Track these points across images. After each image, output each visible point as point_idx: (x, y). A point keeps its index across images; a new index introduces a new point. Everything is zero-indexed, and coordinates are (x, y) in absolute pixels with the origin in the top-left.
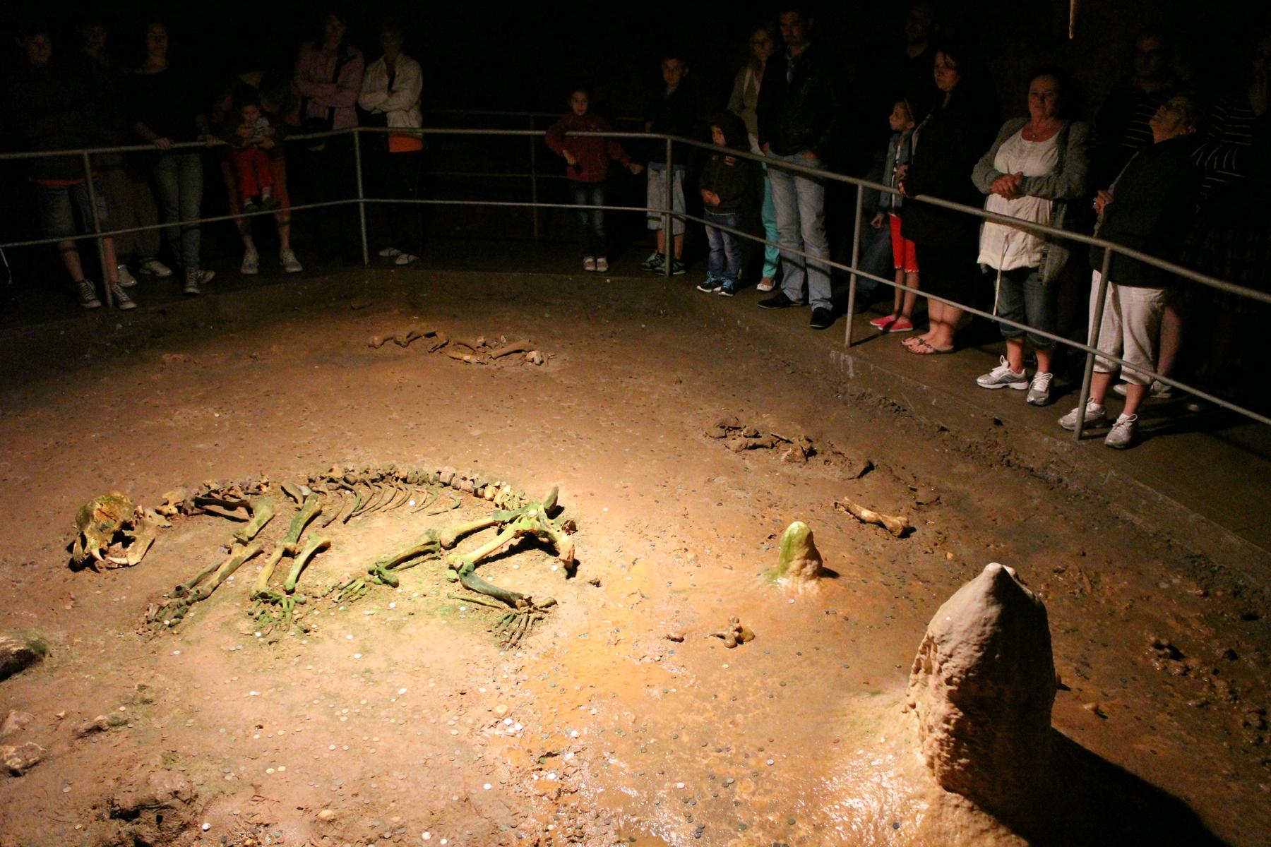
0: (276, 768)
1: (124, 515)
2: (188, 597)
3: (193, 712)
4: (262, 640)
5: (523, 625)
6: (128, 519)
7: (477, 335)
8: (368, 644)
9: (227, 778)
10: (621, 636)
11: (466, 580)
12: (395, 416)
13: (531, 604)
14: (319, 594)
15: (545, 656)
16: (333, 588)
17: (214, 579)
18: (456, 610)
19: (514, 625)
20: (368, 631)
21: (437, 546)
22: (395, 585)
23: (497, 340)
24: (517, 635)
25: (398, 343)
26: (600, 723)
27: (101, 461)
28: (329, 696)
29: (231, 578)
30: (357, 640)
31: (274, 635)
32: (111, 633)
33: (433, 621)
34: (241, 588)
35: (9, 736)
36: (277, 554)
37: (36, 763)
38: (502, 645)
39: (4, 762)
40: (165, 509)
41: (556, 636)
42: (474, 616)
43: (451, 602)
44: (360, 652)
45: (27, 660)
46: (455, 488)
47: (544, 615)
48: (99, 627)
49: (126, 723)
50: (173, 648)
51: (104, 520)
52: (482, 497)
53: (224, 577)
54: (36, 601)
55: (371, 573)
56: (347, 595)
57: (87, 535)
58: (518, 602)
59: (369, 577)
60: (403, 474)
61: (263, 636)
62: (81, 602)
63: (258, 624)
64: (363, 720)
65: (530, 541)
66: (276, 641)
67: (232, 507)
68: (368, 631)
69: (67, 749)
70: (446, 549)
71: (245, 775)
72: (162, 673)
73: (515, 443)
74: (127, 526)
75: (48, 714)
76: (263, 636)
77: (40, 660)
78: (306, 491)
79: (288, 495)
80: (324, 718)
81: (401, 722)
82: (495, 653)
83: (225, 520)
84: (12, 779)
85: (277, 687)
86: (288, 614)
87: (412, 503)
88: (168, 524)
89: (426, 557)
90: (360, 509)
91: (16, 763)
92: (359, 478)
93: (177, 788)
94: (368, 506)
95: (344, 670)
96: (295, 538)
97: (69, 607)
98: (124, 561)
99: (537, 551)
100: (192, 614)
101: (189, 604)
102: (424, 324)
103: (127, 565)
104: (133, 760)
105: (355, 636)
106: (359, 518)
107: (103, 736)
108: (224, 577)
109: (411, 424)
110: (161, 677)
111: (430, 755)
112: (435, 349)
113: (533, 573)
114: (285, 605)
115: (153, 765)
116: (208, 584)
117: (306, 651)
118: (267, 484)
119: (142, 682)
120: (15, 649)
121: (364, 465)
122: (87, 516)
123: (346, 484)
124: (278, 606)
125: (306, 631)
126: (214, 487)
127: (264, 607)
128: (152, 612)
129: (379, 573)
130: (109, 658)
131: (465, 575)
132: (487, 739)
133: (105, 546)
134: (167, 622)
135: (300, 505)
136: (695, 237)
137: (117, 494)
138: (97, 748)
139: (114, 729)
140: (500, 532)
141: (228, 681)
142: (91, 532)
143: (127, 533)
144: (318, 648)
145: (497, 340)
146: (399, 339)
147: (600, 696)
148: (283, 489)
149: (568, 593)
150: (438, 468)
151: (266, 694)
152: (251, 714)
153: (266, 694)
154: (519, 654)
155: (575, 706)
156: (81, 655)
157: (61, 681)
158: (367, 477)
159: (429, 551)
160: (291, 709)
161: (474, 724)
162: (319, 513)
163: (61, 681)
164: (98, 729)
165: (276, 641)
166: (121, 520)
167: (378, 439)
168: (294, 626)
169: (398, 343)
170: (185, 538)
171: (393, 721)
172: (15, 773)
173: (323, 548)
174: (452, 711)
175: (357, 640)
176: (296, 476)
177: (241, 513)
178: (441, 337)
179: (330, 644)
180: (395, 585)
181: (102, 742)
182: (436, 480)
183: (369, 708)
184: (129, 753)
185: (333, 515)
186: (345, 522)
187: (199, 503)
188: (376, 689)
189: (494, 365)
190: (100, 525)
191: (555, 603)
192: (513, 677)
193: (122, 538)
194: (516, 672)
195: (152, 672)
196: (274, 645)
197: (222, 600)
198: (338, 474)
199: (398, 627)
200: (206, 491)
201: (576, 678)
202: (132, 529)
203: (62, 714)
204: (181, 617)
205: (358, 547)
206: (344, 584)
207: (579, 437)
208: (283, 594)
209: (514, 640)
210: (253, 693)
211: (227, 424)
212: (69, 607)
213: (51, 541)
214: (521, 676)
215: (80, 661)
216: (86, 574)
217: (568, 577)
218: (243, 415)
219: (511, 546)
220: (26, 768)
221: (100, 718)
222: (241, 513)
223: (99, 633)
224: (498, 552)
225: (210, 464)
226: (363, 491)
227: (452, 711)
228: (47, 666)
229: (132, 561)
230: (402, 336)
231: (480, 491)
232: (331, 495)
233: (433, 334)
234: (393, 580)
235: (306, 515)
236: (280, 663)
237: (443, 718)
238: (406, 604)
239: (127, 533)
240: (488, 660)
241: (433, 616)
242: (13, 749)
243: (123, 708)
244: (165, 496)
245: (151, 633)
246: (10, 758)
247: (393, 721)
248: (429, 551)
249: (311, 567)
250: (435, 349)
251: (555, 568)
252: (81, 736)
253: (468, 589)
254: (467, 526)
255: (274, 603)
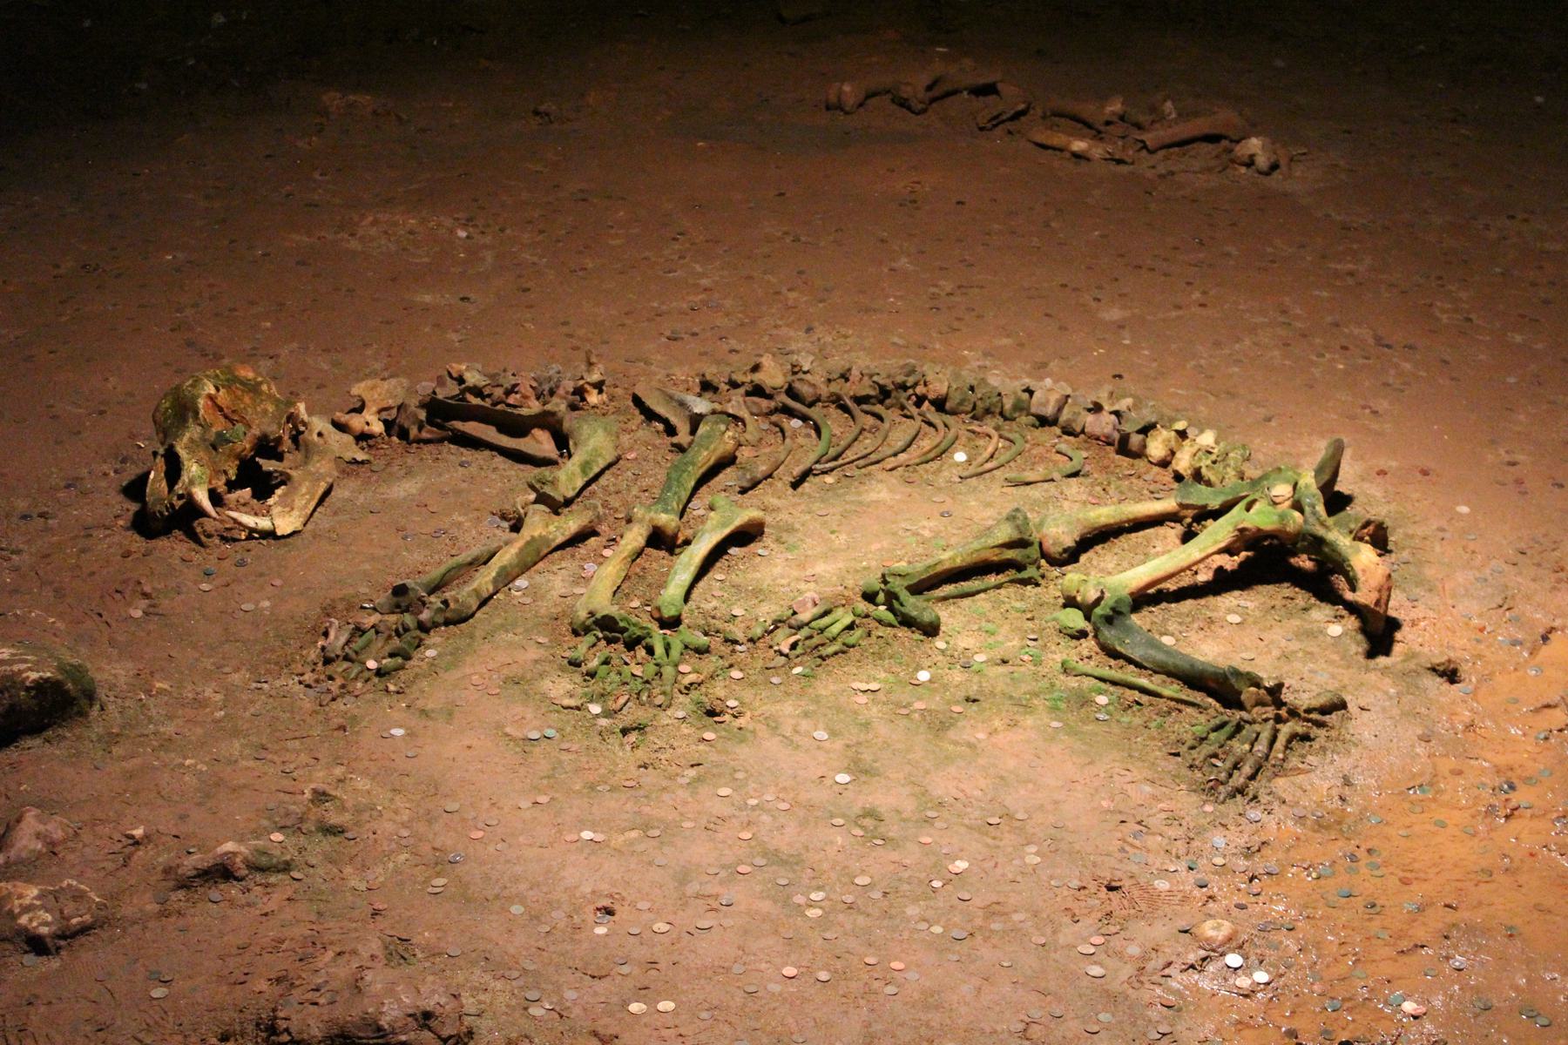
0: (652, 1003)
1: (263, 421)
2: (420, 614)
3: (442, 862)
4: (604, 722)
5: (1261, 747)
6: (273, 430)
7: (1104, 98)
8: (867, 756)
9: (535, 1011)
10: (1516, 798)
11: (1109, 634)
12: (903, 262)
13: (1279, 704)
14: (740, 636)
15: (1320, 825)
16: (778, 623)
17: (484, 579)
18: (1085, 701)
19: (1239, 747)
20: (866, 726)
21: (1034, 552)
22: (931, 630)
23: (1153, 109)
24: (1247, 769)
25: (903, 104)
26: (1476, 990)
27: (189, 312)
28: (775, 858)
29: (521, 582)
30: (839, 744)
31: (633, 714)
32: (236, 678)
33: (1030, 721)
34: (546, 607)
35: (20, 861)
36: (635, 537)
37: (84, 930)
38: (1210, 789)
39: (13, 916)
40: (356, 422)
41: (1347, 782)
42: (1133, 719)
43: (1073, 682)
44: (848, 770)
45: (55, 706)
46: (1068, 431)
47: (1315, 731)
48: (208, 663)
49: (286, 867)
50: (389, 724)
51: (219, 425)
52: (1139, 454)
53: (506, 578)
54: (59, 593)
55: (869, 597)
56: (812, 642)
57: (183, 453)
58: (1249, 693)
59: (863, 606)
60: (938, 387)
61: (608, 714)
62: (165, 603)
63: (595, 686)
64: (861, 919)
65: (1266, 561)
66: (640, 728)
67: (519, 427)
68: (866, 726)
69: (152, 908)
70: (1056, 562)
71: (577, 1011)
72: (365, 773)
73: (1217, 344)
74: (268, 447)
75: (105, 830)
76: (608, 714)
77: (83, 714)
78: (701, 406)
79: (650, 415)
80: (766, 906)
81: (956, 933)
82: (1187, 803)
83: (499, 460)
84: (30, 959)
85: (646, 827)
86: (668, 671)
87: (960, 457)
88: (360, 456)
89: (1001, 578)
90: (833, 461)
91: (42, 922)
92: (824, 391)
93: (429, 1004)
94: (850, 455)
95: (811, 807)
96: (675, 505)
97: (138, 614)
98: (264, 523)
99: (1286, 590)
100: (430, 653)
101: (424, 628)
102: (968, 62)
103: (270, 535)
104: (316, 943)
105: (833, 733)
106: (829, 479)
107: (234, 890)
108: (506, 578)
109: (948, 286)
110: (362, 783)
111: (1036, 1014)
112: (996, 121)
113: (1280, 635)
114: (659, 650)
115: (365, 954)
116: (468, 589)
117: (714, 757)
118: (599, 386)
119: (321, 787)
120: (34, 676)
121: (837, 363)
122: (183, 410)
123: (792, 404)
124: (641, 652)
125: (711, 713)
126: (473, 378)
127: (604, 650)
128: (337, 639)
129: (891, 597)
130: (236, 733)
131: (1109, 620)
132: (1177, 993)
133: (220, 485)
134: (372, 664)
135: (683, 437)
136: (799, 628)
137: (247, 373)
138: (223, 917)
139: (259, 877)
140: (1187, 537)
141: (525, 804)
142: (192, 446)
143: (268, 465)
144: (743, 751)
145: (1153, 109)
146: (906, 92)
147: (1471, 929)
148: (637, 401)
149: (1373, 690)
150: (1028, 381)
151: (619, 840)
152: (585, 879)
153: (619, 840)
154: (1254, 814)
155: (1405, 944)
156: (170, 718)
157: (129, 765)
158: (847, 390)
159: (1012, 562)
160: (683, 878)
161: (1144, 958)
162: (727, 461)
163: (129, 765)
164: (222, 872)
165: (640, 728)
166: (256, 431)
167: (867, 310)
168: (682, 698)
169: (903, 104)
170: (405, 489)
171: (937, 929)
172: (37, 945)
173: (746, 536)
174: (1088, 923)
175: (839, 744)
176: (669, 378)
177: (541, 443)
178: (1011, 96)
179: (772, 745)
180: (931, 630)
181: (232, 902)
182: (1020, 407)
183: (877, 895)
184: (301, 931)
185: (764, 468)
186: (795, 485)
187: (439, 412)
188: (895, 856)
189: (1148, 167)
190: (212, 435)
191: (1342, 705)
192: (1242, 863)
193: (258, 481)
194: (1248, 853)
195: (339, 771)
196: (633, 737)
197: (503, 627)
198: (773, 375)
199: (940, 725)
200: (452, 389)
201: (1405, 882)
202: (279, 457)
203: (138, 832)
204: (408, 658)
205: (827, 547)
206: (804, 616)
207: (1379, 341)
208: (654, 626)
209: (1238, 779)
210: (587, 835)
211: (489, 256)
212: (138, 614)
213: (84, 472)
214: (1259, 865)
215: (169, 729)
216: (174, 547)
217: (1371, 654)
218: (526, 237)
219: (1220, 570)
220: (63, 937)
221: (230, 846)
222: (541, 443)
223: (207, 676)
224: (1186, 581)
225: (454, 337)
226: (834, 423)
227: (1088, 923)
228: (98, 729)
229: (285, 525)
230: (916, 83)
231: (1135, 440)
232: (756, 427)
233: (989, 90)
234: (927, 617)
235: (704, 457)
236: (649, 777)
237: (1068, 933)
238: (957, 676)
239: (268, 465)
240: (1173, 819)
241: (1027, 708)
242: (35, 892)
243: (277, 837)
244: (358, 389)
245: (334, 687)
246: (27, 909)
247: (937, 929)
248: (1012, 562)
249: (716, 574)
250: (996, 121)
251: (1335, 630)
252: (184, 884)
253: (1113, 654)
254: (1106, 514)
255: (631, 645)
